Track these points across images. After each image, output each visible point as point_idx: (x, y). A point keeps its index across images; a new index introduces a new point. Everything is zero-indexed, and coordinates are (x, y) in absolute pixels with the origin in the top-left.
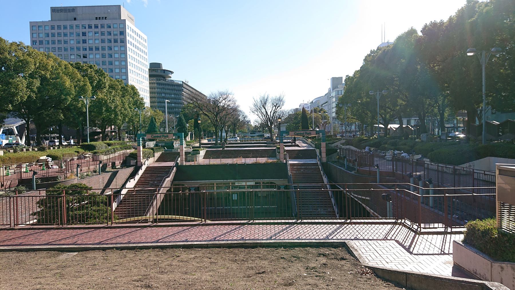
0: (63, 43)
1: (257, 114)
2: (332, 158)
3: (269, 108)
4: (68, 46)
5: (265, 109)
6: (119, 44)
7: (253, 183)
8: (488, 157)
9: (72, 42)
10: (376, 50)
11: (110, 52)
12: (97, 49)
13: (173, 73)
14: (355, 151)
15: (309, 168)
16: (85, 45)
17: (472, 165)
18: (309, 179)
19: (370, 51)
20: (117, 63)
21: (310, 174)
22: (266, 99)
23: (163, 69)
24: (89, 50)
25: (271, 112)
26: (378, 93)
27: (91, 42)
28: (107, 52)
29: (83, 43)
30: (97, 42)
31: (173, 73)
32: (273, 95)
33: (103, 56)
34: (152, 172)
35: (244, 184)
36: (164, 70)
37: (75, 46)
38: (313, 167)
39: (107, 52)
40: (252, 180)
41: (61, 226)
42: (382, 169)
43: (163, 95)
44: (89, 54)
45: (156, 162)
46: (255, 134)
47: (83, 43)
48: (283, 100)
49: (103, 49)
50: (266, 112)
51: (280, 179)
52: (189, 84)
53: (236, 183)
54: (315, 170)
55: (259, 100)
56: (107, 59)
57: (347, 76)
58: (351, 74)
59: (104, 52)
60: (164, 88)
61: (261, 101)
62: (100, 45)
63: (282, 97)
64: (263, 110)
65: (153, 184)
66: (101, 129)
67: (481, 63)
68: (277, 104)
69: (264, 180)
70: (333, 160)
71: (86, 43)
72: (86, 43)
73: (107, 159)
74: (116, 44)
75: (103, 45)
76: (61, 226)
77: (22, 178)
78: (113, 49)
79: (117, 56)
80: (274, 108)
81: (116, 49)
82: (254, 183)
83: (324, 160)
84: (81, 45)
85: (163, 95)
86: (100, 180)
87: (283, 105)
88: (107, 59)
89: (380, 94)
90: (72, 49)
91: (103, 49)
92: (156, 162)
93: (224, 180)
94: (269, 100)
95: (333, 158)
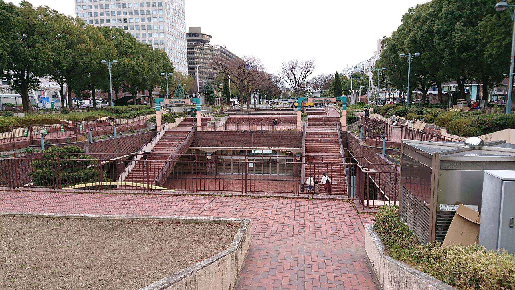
0: (104, 7)
1: (286, 80)
2: (353, 127)
3: (298, 73)
4: (109, 10)
5: (294, 75)
6: (157, 7)
7: (269, 152)
8: (509, 129)
9: (113, 6)
10: (414, 8)
11: (149, 16)
12: (137, 13)
13: (212, 37)
14: (374, 120)
15: (327, 137)
16: (125, 9)
17: (489, 137)
18: (329, 148)
19: (408, 9)
20: (156, 28)
21: (327, 143)
22: (295, 63)
23: (202, 33)
24: (129, 15)
25: (299, 78)
26: (410, 56)
27: (130, 6)
28: (146, 16)
29: (123, 7)
30: (136, 5)
31: (212, 37)
32: (302, 59)
33: (143, 20)
34: (319, 146)
35: (260, 152)
36: (203, 35)
37: (116, 11)
38: (331, 136)
39: (146, 16)
40: (268, 148)
41: (296, 196)
42: (398, 140)
43: (201, 60)
44: (129, 18)
45: (178, 127)
46: (287, 100)
47: (123, 7)
48: (314, 64)
49: (143, 12)
50: (295, 78)
51: (296, 148)
52: (226, 48)
53: (253, 150)
54: (333, 139)
55: (288, 65)
56: (146, 24)
57: (384, 37)
58: (389, 35)
59: (144, 16)
60: (202, 53)
61: (290, 66)
62: (140, 9)
63: (312, 62)
64: (292, 76)
65: (169, 148)
66: (132, 94)
67: (512, 20)
68: (306, 69)
69: (279, 148)
70: (354, 129)
71: (126, 7)
72: (126, 7)
73: (138, 121)
74: (154, 8)
75: (142, 9)
76: (296, 196)
77: (33, 139)
78: (151, 13)
79: (155, 20)
80: (304, 72)
81: (155, 12)
82: (271, 151)
83: (344, 129)
84: (122, 9)
85: (201, 60)
86: (116, 143)
87: (313, 69)
88: (146, 24)
89: (411, 56)
90: (113, 13)
91: (143, 12)
92: (178, 127)
93: (240, 148)
94: (299, 65)
95: (354, 126)
